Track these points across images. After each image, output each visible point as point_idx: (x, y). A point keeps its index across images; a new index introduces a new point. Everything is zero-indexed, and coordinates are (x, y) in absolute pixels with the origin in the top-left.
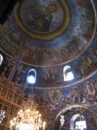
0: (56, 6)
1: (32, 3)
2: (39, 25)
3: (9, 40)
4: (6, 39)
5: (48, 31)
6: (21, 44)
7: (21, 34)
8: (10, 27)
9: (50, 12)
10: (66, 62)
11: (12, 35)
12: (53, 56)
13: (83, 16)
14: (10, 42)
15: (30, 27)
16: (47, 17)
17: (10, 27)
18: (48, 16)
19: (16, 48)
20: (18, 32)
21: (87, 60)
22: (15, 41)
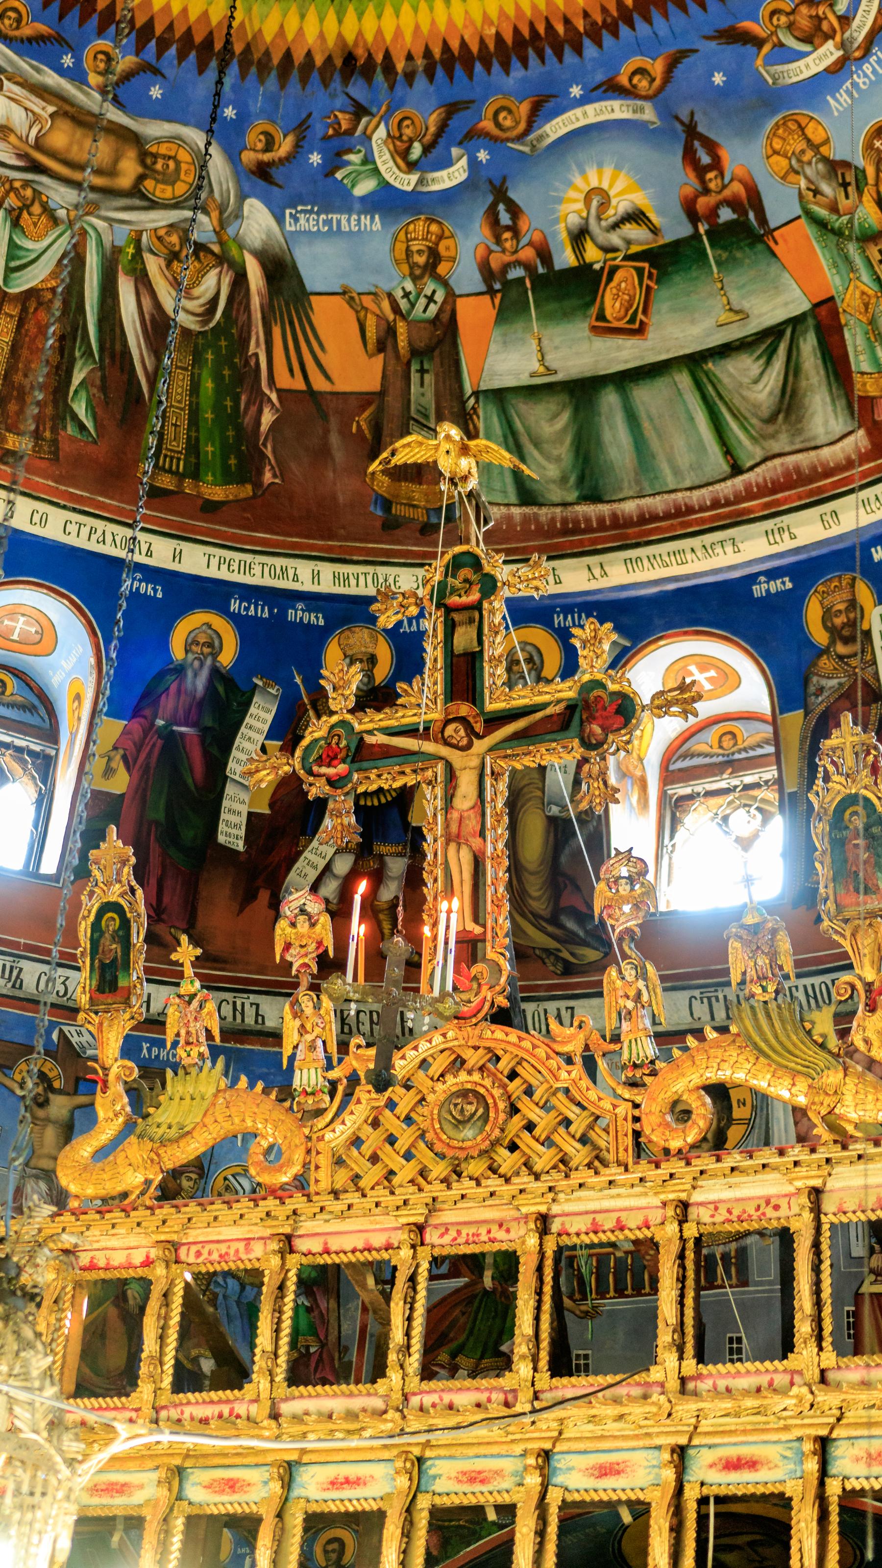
3: (577, 350)
4: (531, 391)
6: (780, 204)
7: (612, 89)
8: (386, 201)
11: (545, 254)
14: (625, 353)
17: (386, 201)
19: (774, 333)
20: (556, 128)
22: (664, 261)
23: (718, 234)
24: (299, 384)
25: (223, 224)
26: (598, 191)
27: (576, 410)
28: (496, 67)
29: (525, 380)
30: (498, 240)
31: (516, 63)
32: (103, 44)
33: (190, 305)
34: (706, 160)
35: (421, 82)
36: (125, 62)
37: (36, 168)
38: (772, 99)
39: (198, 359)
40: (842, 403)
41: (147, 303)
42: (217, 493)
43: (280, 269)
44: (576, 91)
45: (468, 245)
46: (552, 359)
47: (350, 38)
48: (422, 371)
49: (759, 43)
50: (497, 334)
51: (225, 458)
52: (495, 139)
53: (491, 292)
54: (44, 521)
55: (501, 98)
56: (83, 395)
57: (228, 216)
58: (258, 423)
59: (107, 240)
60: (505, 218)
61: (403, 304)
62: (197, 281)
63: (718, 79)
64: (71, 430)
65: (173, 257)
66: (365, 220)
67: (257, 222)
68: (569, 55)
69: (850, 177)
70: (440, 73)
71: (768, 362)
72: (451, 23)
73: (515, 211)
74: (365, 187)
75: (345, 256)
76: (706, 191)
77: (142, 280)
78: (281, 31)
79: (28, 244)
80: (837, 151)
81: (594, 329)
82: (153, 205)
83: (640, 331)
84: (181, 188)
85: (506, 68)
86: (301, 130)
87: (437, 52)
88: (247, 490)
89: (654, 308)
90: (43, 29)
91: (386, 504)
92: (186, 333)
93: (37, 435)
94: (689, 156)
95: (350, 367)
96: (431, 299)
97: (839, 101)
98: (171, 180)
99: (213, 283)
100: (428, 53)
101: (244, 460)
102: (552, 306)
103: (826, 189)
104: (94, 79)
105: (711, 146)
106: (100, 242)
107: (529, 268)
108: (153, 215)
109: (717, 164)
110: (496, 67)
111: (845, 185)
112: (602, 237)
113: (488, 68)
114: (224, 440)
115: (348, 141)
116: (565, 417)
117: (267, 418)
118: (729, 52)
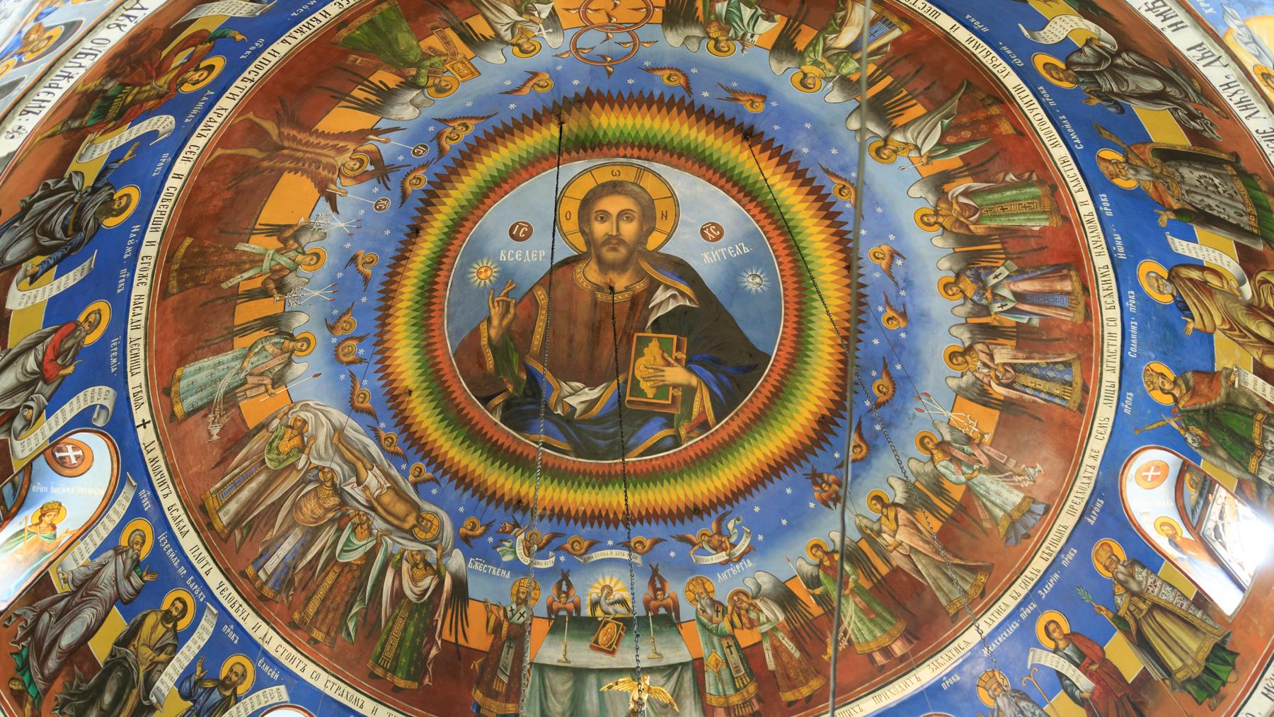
0: (614, 188)
1: (489, 320)
2: (675, 386)
3: (583, 655)
4: (557, 669)
5: (757, 361)
6: (687, 611)
7: (626, 546)
8: (515, 567)
9: (637, 250)
10: (1097, 445)
12: (969, 490)
13: (784, 46)
14: (603, 661)
15: (641, 449)
16: (660, 295)
18: (653, 286)
19: (673, 667)
20: (597, 555)
21: (1195, 275)
22: (627, 623)
23: (657, 618)
24: (453, 640)
25: (442, 556)
26: (610, 589)
27: (575, 682)
28: (579, 524)
29: (555, 663)
30: (559, 597)
31: (588, 524)
32: (422, 465)
33: (416, 590)
34: (659, 586)
35: (546, 520)
36: (427, 474)
37: (373, 509)
38: (693, 568)
39: (411, 616)
40: (699, 706)
41: (397, 583)
42: (401, 683)
43: (460, 587)
44: (610, 543)
45: (545, 596)
46: (569, 656)
47: (523, 493)
48: (509, 647)
49: (694, 545)
50: (548, 638)
51: (409, 666)
52: (569, 553)
53: (549, 618)
54: (317, 678)
55: (578, 535)
56: (354, 620)
57: (445, 554)
58: (429, 652)
59: (390, 549)
60: (564, 588)
61: (509, 614)
62: (422, 580)
63: (672, 554)
64: (344, 635)
65: (415, 565)
66: (504, 572)
67: (456, 560)
68: (612, 527)
69: (720, 609)
70: (555, 519)
71: (668, 680)
72: (567, 500)
73: (570, 586)
74: (507, 558)
75: (489, 588)
76: (656, 599)
77: (398, 573)
78: (495, 483)
79: (355, 541)
80: (717, 597)
81: (592, 647)
82: (415, 540)
83: (612, 652)
84: (429, 536)
85: (584, 525)
86: (488, 526)
87: (557, 510)
88: (415, 685)
89: (621, 644)
90: (399, 450)
91: (479, 708)
92: (410, 601)
93: (328, 634)
94: (652, 583)
95: (478, 638)
96: (522, 615)
97: (723, 577)
98: (426, 531)
99: (428, 582)
100: (552, 510)
101: (416, 673)
102: (576, 632)
103: (709, 611)
104: (411, 478)
105: (662, 581)
106: (386, 550)
107: (569, 612)
108: (413, 544)
109: (663, 589)
110: (579, 524)
111: (717, 612)
112: (605, 607)
113: (576, 522)
114: (411, 656)
115: (507, 536)
116: (570, 684)
117: (434, 652)
118: (680, 545)
